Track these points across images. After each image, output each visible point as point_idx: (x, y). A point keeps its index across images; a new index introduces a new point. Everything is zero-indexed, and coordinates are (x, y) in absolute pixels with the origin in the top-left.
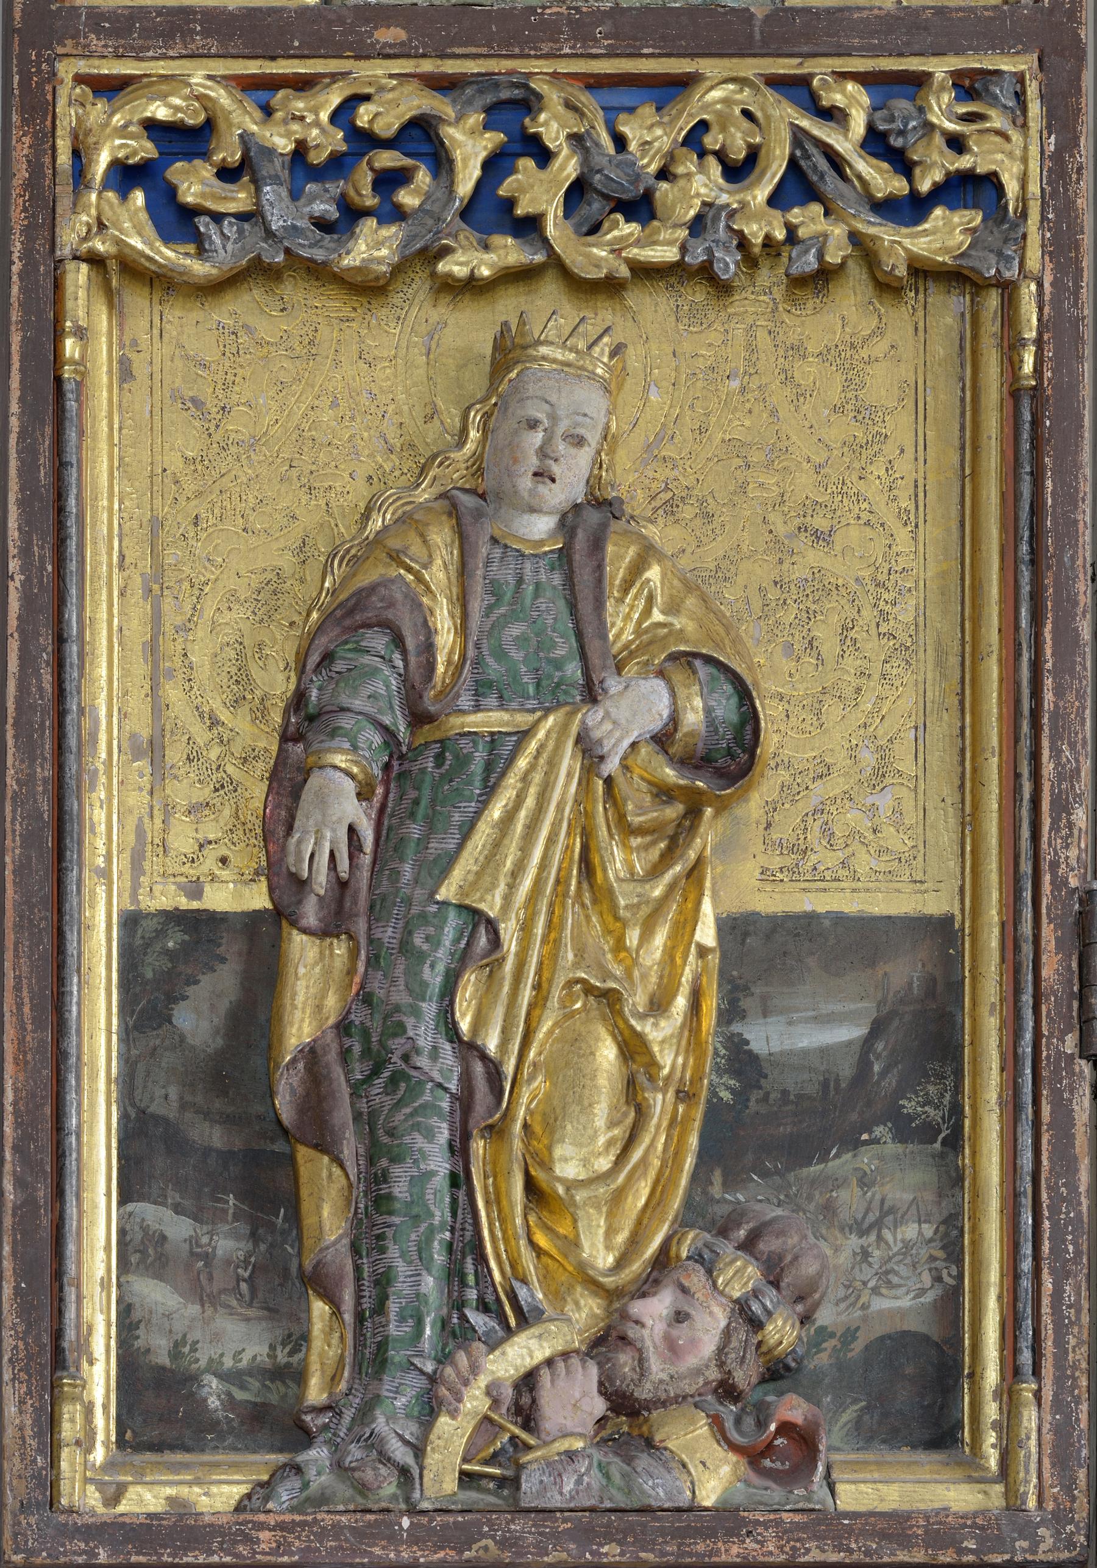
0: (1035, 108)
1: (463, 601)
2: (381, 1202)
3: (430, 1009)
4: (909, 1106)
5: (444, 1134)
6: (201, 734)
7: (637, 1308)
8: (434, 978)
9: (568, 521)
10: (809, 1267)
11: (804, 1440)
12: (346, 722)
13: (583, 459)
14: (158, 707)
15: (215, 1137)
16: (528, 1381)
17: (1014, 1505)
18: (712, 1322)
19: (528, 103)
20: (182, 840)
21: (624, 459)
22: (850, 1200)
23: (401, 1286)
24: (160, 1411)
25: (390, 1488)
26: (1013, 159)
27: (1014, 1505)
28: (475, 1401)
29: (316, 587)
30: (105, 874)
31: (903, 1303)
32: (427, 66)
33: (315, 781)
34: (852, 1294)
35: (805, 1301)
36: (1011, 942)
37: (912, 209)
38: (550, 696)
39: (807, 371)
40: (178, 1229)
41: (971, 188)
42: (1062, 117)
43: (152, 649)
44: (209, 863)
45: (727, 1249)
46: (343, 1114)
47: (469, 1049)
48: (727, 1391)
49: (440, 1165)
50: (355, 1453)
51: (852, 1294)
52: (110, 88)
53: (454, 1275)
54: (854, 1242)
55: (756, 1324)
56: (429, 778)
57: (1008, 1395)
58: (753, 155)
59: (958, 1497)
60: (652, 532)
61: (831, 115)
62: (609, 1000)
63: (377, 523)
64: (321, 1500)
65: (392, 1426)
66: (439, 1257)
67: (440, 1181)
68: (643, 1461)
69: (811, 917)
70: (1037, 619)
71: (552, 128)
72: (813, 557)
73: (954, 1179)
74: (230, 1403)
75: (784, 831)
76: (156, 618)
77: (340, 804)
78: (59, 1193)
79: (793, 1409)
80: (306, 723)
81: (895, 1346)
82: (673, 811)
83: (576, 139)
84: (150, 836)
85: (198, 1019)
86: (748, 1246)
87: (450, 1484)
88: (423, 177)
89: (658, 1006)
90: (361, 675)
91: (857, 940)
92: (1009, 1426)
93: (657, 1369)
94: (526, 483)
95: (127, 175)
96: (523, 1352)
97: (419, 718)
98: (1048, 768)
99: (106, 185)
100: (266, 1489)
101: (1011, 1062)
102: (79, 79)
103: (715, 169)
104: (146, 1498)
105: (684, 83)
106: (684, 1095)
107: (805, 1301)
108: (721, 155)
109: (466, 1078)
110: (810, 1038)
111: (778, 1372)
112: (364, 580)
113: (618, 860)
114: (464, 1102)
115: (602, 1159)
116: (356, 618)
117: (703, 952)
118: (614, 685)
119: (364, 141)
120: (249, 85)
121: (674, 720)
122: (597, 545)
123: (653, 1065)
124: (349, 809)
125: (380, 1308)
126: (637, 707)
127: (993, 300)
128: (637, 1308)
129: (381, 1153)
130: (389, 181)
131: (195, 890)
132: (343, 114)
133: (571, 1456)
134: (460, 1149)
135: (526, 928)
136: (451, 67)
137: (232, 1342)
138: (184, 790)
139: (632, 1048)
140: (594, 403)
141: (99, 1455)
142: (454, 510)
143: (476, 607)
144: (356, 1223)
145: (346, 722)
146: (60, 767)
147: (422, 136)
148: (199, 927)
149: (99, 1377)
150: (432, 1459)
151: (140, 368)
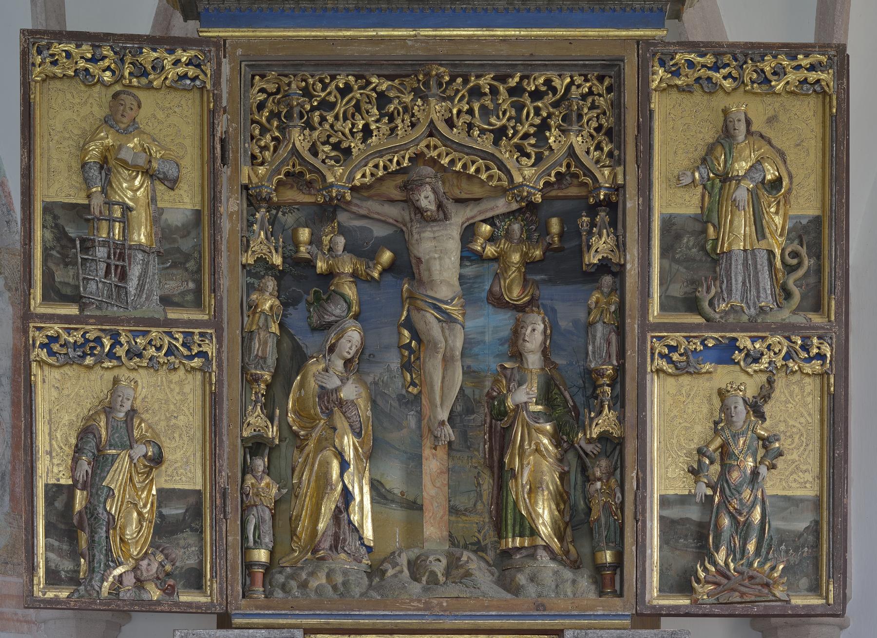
0: (214, 339)
1: (107, 429)
2: (93, 541)
3: (101, 505)
4: (193, 525)
5: (105, 529)
6: (58, 450)
7: (141, 563)
8: (102, 500)
9: (127, 414)
10: (174, 556)
11: (173, 587)
12: (85, 451)
13: (130, 403)
16: (121, 576)
17: (212, 601)
18: (155, 566)
19: (119, 335)
20: (56, 470)
21: (138, 401)
22: (182, 542)
23: (97, 557)
24: (53, 578)
25: (95, 595)
26: (210, 349)
27: (212, 601)
28: (111, 579)
29: (80, 424)
30: (41, 477)
31: (192, 562)
32: (99, 327)
33: (80, 462)
36: (211, 493)
37: (191, 358)
38: (123, 447)
39: (172, 386)
40: (56, 544)
41: (202, 354)
42: (220, 342)
43: (50, 434)
44: (61, 475)
45: (158, 552)
46: (86, 524)
47: (109, 513)
48: (158, 578)
49: (104, 535)
50: (89, 588)
52: (39, 329)
53: (107, 555)
54: (183, 550)
55: (163, 567)
56: (101, 463)
58: (161, 346)
59: (203, 599)
60: (143, 416)
61: (176, 339)
62: (136, 505)
63: (91, 413)
64: (83, 596)
65: (96, 584)
66: (104, 552)
67: (104, 538)
68: (142, 591)
69: (174, 489)
70: (215, 436)
71: (123, 339)
72: (173, 421)
73: (201, 539)
74: (66, 576)
75: (169, 473)
76: (50, 428)
77: (85, 466)
78: (33, 537)
79: (171, 582)
80: (78, 450)
81: (191, 570)
82: (147, 469)
83: (128, 342)
84: (52, 468)
85: (59, 504)
86: (162, 552)
87: (106, 595)
88: (99, 349)
89: (145, 506)
90: (88, 442)
92: (211, 586)
93: (145, 574)
94: (119, 407)
95: (43, 346)
97: (99, 451)
98: (217, 464)
99: (39, 347)
100: (72, 594)
101: (211, 519)
102: (34, 327)
103: (154, 349)
104: (50, 595)
105: (149, 332)
106: (151, 522)
107: (173, 562)
108: (155, 346)
109: (109, 518)
110: (174, 512)
111: (168, 575)
112: (88, 424)
113: (136, 479)
114: (108, 523)
115: (135, 531)
116: (86, 432)
117: (153, 495)
118: (135, 446)
119: (87, 341)
120: (65, 329)
121: (147, 453)
122: (132, 419)
123: (144, 517)
124: (86, 467)
125: (93, 561)
126: (140, 450)
127: (208, 374)
128: (141, 563)
129: (93, 532)
131: (58, 480)
132: (83, 336)
133: (129, 590)
134: (107, 532)
135: (119, 491)
136: (104, 327)
137: (67, 565)
138: (55, 461)
139: (140, 514)
140: (132, 392)
141: (42, 586)
142: (105, 412)
143: (109, 431)
144: (88, 545)
145: (85, 451)
146: (32, 457)
147: (98, 340)
148: (59, 487)
149: (41, 572)
150: (103, 589)
151: (47, 381)
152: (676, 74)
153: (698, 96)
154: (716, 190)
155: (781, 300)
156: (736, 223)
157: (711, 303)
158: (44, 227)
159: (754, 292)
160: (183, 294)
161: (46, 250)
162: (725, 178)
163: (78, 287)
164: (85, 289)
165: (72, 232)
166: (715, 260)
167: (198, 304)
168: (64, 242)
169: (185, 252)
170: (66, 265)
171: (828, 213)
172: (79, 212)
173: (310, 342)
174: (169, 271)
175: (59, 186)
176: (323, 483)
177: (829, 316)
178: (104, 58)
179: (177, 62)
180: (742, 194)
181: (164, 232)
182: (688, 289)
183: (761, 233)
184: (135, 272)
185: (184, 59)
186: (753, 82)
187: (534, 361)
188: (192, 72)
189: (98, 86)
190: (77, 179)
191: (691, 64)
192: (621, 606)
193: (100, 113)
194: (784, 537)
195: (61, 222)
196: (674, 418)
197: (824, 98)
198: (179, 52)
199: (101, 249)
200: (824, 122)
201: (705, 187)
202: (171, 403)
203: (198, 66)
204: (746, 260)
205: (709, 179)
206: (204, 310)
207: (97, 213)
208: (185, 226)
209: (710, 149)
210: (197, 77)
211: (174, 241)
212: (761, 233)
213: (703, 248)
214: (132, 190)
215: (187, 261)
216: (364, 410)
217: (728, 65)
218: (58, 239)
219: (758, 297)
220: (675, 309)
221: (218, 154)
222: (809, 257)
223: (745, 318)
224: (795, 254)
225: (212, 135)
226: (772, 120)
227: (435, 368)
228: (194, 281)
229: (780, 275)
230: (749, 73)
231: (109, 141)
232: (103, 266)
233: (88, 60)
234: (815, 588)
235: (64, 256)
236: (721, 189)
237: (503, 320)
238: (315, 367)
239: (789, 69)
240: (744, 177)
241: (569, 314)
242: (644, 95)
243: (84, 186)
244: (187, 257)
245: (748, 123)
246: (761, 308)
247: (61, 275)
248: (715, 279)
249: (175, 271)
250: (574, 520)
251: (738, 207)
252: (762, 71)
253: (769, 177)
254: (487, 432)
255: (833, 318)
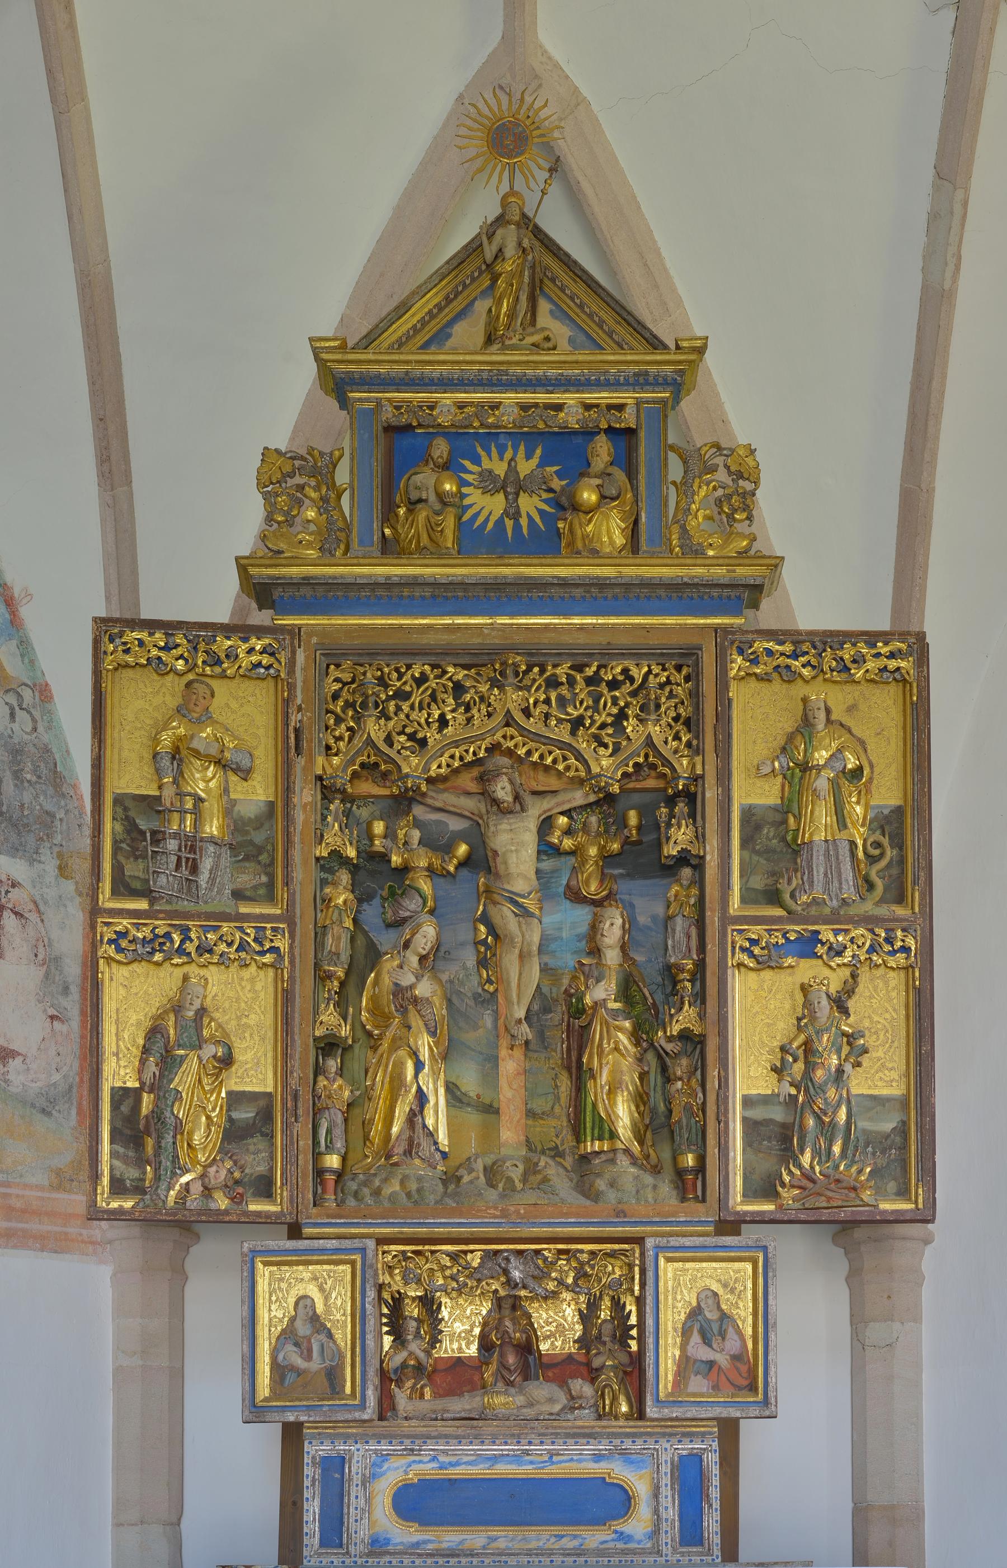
8: (169, 1103)
9: (197, 1012)
14: (118, 1046)
15: (128, 1132)
16: (188, 1184)
18: (223, 1173)
19: (189, 930)
21: (209, 999)
22: (252, 1148)
24: (118, 1187)
28: (177, 1187)
29: (148, 1024)
31: (262, 1169)
34: (252, 1167)
35: (242, 1169)
37: (262, 953)
39: (243, 983)
40: (121, 1150)
42: (292, 936)
46: (152, 1129)
47: (177, 1117)
48: (226, 1186)
51: (252, 1167)
53: (173, 1162)
56: (169, 1063)
57: (281, 1188)
61: (247, 934)
65: (161, 1192)
71: (193, 935)
73: (272, 1145)
77: (152, 1067)
79: (240, 1190)
80: (146, 1051)
81: (261, 1177)
84: (119, 1072)
85: (125, 1109)
89: (214, 1109)
91: (254, 1096)
92: (281, 1194)
95: (110, 942)
96: (185, 1179)
97: (167, 1051)
100: (137, 1204)
107: (242, 1169)
111: (237, 1182)
113: (205, 1081)
116: (154, 1032)
119: (157, 936)
124: (153, 1068)
126: (209, 1050)
130: (162, 944)
132: (152, 931)
134: (174, 1137)
137: (132, 1173)
139: (208, 1117)
147: (168, 935)
149: (106, 1180)
152: (755, 661)
153: (777, 685)
154: (797, 780)
155: (863, 891)
156: (816, 813)
157: (793, 896)
158: (114, 819)
159: (836, 884)
160: (255, 888)
161: (115, 843)
162: (805, 767)
163: (148, 881)
164: (155, 882)
165: (143, 824)
166: (795, 850)
167: (271, 898)
168: (134, 835)
169: (256, 844)
170: (136, 858)
171: (910, 802)
172: (150, 804)
173: (385, 940)
174: (241, 864)
175: (131, 778)
176: (397, 1084)
177: (913, 908)
178: (177, 646)
179: (251, 651)
180: (822, 783)
181: (237, 825)
182: (770, 881)
183: (842, 823)
184: (206, 865)
185: (258, 648)
186: (832, 670)
187: (612, 957)
188: (266, 660)
189: (171, 675)
190: (148, 770)
191: (769, 652)
192: (706, 1213)
193: (173, 702)
194: (871, 1139)
195: (132, 814)
196: (756, 1014)
197: (904, 687)
198: (254, 640)
199: (172, 841)
200: (904, 711)
201: (785, 777)
202: (242, 1000)
203: (272, 654)
204: (828, 850)
205: (789, 769)
206: (277, 904)
207: (168, 805)
208: (258, 818)
209: (790, 738)
210: (271, 666)
211: (247, 833)
212: (842, 823)
213: (783, 839)
214: (204, 781)
215: (260, 853)
216: (439, 1009)
217: (807, 653)
218: (128, 832)
219: (841, 889)
220: (755, 902)
221: (292, 744)
222: (892, 848)
223: (827, 911)
224: (877, 845)
225: (287, 725)
226: (851, 709)
227: (510, 962)
228: (266, 874)
229: (862, 866)
230: (828, 660)
231: (182, 731)
232: (174, 859)
233: (161, 649)
234: (903, 1193)
235: (135, 849)
236: (801, 778)
237: (581, 915)
238: (389, 964)
239: (868, 657)
240: (824, 766)
241: (649, 909)
242: (722, 684)
243: (155, 777)
244: (260, 849)
245: (828, 711)
246: (843, 899)
247: (133, 869)
248: (796, 871)
249: (247, 864)
250: (656, 1124)
251: (818, 796)
252: (842, 659)
253: (850, 766)
254: (566, 1030)
255: (917, 910)
